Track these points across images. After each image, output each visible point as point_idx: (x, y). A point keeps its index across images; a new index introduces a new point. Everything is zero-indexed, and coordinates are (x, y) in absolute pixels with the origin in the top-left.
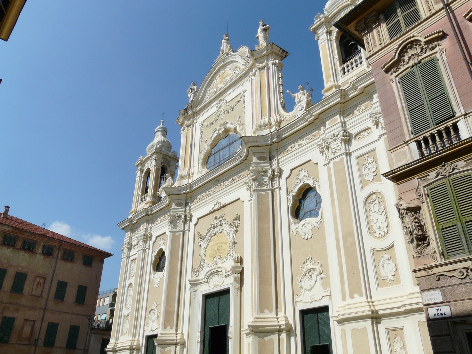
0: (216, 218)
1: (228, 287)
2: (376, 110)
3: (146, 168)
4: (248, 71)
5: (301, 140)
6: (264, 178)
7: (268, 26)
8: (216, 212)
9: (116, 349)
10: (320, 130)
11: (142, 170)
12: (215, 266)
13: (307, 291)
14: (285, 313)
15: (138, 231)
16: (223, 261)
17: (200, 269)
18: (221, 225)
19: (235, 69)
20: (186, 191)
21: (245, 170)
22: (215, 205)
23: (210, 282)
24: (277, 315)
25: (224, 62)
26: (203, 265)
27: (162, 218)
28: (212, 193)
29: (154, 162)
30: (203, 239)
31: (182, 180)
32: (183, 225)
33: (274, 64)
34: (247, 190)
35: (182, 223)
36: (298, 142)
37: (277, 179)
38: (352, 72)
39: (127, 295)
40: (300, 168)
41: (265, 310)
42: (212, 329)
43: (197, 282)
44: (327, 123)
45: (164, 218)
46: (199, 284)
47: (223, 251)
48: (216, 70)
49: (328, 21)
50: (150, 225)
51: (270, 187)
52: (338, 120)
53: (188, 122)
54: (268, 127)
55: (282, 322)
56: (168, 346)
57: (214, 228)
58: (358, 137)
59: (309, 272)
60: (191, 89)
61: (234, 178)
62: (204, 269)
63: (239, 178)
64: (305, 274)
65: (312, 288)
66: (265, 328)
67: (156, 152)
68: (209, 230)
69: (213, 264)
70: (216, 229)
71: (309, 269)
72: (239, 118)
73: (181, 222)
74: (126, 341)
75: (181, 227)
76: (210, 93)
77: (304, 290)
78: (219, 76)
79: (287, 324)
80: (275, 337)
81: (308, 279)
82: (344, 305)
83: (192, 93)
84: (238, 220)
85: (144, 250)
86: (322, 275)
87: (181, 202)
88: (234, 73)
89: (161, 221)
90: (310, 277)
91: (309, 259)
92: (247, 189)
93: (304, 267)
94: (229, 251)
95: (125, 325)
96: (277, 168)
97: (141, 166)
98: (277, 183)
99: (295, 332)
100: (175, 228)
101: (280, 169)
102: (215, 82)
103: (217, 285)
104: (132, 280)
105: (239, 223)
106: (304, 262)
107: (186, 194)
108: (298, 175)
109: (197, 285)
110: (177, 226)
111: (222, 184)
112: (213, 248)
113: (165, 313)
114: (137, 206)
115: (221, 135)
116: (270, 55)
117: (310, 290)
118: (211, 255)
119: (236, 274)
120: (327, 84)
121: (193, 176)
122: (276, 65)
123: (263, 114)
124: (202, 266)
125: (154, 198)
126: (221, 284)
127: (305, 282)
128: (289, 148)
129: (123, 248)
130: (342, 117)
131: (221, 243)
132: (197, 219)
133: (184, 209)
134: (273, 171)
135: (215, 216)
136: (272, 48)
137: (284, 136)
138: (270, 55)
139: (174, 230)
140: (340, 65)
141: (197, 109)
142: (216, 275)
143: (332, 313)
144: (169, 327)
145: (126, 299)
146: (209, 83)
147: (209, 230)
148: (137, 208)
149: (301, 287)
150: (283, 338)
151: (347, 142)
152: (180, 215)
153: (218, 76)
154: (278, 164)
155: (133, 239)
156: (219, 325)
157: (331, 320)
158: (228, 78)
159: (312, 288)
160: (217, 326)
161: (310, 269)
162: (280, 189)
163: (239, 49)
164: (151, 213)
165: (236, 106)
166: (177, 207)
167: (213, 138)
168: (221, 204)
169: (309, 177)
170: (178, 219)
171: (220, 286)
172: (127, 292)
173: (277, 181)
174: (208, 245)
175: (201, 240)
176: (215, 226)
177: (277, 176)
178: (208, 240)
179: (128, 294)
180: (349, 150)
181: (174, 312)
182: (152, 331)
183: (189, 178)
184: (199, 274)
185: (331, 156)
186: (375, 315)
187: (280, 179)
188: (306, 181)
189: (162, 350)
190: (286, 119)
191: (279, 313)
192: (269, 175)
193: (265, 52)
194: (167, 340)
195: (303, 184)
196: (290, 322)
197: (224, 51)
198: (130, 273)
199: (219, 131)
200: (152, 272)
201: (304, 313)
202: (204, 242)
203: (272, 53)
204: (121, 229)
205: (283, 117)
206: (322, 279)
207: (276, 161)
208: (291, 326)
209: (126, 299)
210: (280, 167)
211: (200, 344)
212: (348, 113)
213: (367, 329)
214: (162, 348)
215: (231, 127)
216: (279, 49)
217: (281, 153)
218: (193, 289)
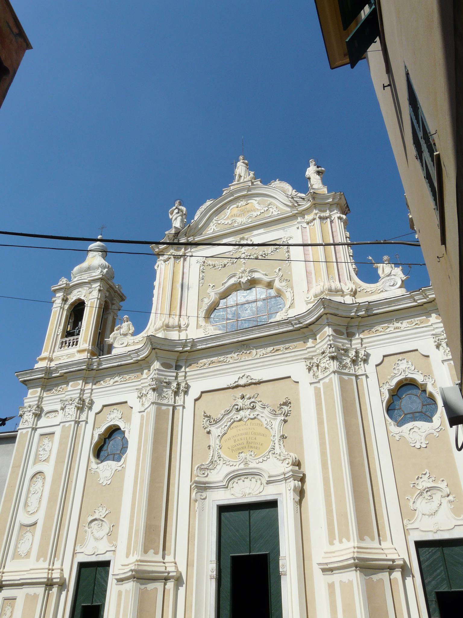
0: (243, 397)
1: (275, 498)
2: (67, 397)
3: (74, 298)
4: (296, 215)
5: (398, 322)
6: (343, 358)
7: (323, 169)
8: (240, 388)
9: (4, 583)
10: (68, 385)
11: (65, 299)
12: (242, 466)
13: (427, 517)
14: (62, 565)
15: (56, 390)
16: (261, 460)
17: (210, 467)
18: (253, 408)
19: (269, 205)
20: (183, 348)
21: (299, 341)
22: (239, 378)
23: (233, 487)
24: (164, 558)
25: (248, 191)
26: (215, 461)
27: (117, 379)
28: (231, 361)
29: (95, 294)
30: (216, 423)
31: (167, 331)
32: (173, 396)
33: (340, 218)
34: (138, 398)
35: (172, 393)
36: (393, 324)
37: (87, 410)
38: (74, 348)
39: (29, 491)
40: (400, 357)
41: (366, 537)
42: (235, 559)
43: (207, 485)
44: (71, 384)
45: (122, 380)
46: (210, 488)
47: (258, 446)
48: (232, 198)
49: (68, 288)
50: (89, 386)
51: (171, 402)
52: (38, 393)
53: (175, 252)
54: (340, 294)
55: (171, 568)
56: (153, 581)
57: (238, 410)
58: (48, 415)
59: (427, 491)
60: (176, 208)
61: (276, 347)
62: (218, 467)
63: (286, 349)
64: (421, 494)
65: (434, 513)
66: (374, 562)
67: (102, 280)
68: (228, 412)
69: (240, 462)
70: (241, 412)
71: (428, 488)
72: (279, 270)
73: (170, 392)
74: (31, 570)
75: (170, 399)
76: (219, 224)
77: (421, 515)
78: (237, 207)
79: (62, 578)
80: (159, 585)
81: (425, 501)
82: (29, 569)
83: (179, 214)
84: (288, 406)
85: (77, 423)
86: (451, 498)
87: (169, 362)
88: (267, 210)
89: (114, 383)
90: (429, 498)
91: (425, 474)
92: (138, 396)
93: (418, 484)
94: (273, 447)
95: (21, 542)
96: (89, 399)
97: (64, 293)
98: (85, 415)
99: (67, 588)
100: (161, 399)
101: (92, 400)
102: (228, 212)
103: (250, 494)
104: (48, 469)
105: (290, 411)
106: (418, 477)
107: (180, 353)
108: (396, 365)
109: (207, 489)
110: (165, 396)
111: (254, 352)
112: (239, 438)
113: (146, 527)
114: (54, 352)
115: (242, 284)
116: (335, 206)
117: (432, 515)
118: (234, 448)
119: (296, 482)
120: (83, 345)
121: (186, 330)
122: (342, 220)
123: (330, 276)
124: (214, 462)
125: (94, 346)
126: (258, 492)
127: (421, 503)
128: (379, 328)
129: (23, 412)
130: (43, 391)
131: (255, 434)
132: (200, 393)
133: (175, 374)
134: (178, 385)
135: (242, 394)
136: (340, 198)
137: (375, 312)
138: (335, 206)
139: (159, 401)
140: (62, 337)
141: (196, 240)
142: (246, 478)
143: (113, 570)
144: (151, 551)
145: (27, 497)
146: (216, 210)
147: (228, 412)
148: (53, 354)
149: (416, 510)
150: (396, 579)
151: (38, 416)
152: (169, 382)
153: (235, 206)
154: (91, 394)
155: (77, 393)
156: (251, 554)
157: (110, 577)
158: (255, 214)
159: (434, 513)
160: (248, 554)
161: (430, 488)
162: (87, 423)
163: (274, 182)
164: (98, 367)
165: (272, 253)
166: (162, 369)
167: (227, 285)
168: (252, 379)
169: (416, 370)
170: (166, 387)
171: (256, 496)
172: (30, 486)
173: (86, 412)
174: (225, 434)
175: (210, 425)
176: (241, 407)
177: (87, 406)
178: (226, 426)
179: (31, 489)
180: (36, 425)
181: (160, 526)
182: (94, 555)
183: (180, 331)
184: (209, 473)
185: (321, 376)
186: (50, 582)
187: (186, 396)
188: (409, 374)
189: (143, 587)
190: (365, 291)
191: (166, 557)
192: (172, 388)
193: (331, 200)
194: (153, 572)
195: (404, 377)
196: (65, 576)
197: (241, 176)
198: (36, 455)
199: (239, 278)
200: (92, 459)
201: (82, 566)
202: (217, 428)
203: (338, 204)
204: (21, 381)
205: (359, 288)
206: (450, 502)
207: (184, 374)
208: (65, 580)
209: (27, 497)
210: (92, 398)
211: (216, 581)
212: (49, 389)
213: (382, 579)
214: (141, 584)
215: (262, 278)
216: (345, 202)
217: (363, 331)
218: (201, 495)
